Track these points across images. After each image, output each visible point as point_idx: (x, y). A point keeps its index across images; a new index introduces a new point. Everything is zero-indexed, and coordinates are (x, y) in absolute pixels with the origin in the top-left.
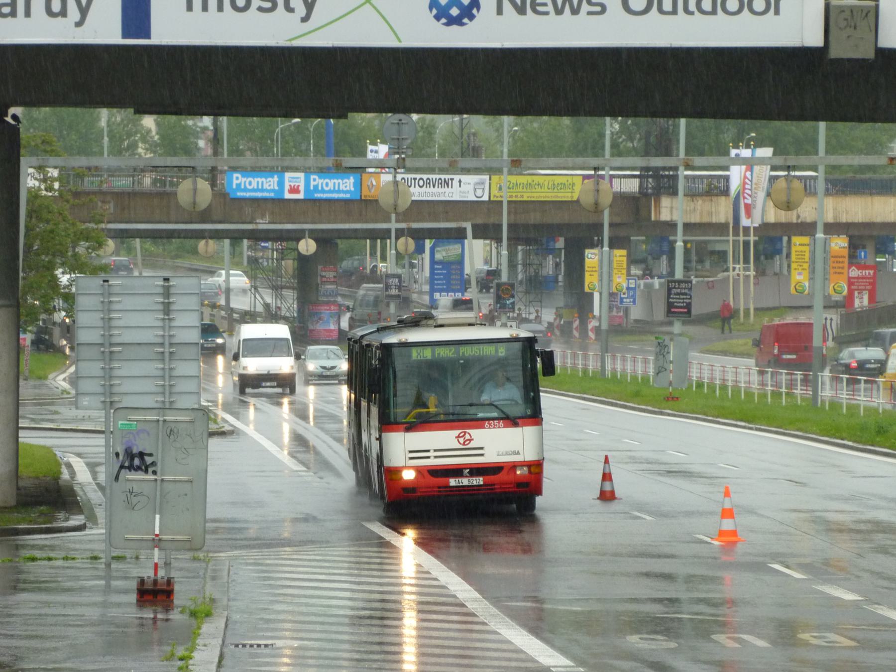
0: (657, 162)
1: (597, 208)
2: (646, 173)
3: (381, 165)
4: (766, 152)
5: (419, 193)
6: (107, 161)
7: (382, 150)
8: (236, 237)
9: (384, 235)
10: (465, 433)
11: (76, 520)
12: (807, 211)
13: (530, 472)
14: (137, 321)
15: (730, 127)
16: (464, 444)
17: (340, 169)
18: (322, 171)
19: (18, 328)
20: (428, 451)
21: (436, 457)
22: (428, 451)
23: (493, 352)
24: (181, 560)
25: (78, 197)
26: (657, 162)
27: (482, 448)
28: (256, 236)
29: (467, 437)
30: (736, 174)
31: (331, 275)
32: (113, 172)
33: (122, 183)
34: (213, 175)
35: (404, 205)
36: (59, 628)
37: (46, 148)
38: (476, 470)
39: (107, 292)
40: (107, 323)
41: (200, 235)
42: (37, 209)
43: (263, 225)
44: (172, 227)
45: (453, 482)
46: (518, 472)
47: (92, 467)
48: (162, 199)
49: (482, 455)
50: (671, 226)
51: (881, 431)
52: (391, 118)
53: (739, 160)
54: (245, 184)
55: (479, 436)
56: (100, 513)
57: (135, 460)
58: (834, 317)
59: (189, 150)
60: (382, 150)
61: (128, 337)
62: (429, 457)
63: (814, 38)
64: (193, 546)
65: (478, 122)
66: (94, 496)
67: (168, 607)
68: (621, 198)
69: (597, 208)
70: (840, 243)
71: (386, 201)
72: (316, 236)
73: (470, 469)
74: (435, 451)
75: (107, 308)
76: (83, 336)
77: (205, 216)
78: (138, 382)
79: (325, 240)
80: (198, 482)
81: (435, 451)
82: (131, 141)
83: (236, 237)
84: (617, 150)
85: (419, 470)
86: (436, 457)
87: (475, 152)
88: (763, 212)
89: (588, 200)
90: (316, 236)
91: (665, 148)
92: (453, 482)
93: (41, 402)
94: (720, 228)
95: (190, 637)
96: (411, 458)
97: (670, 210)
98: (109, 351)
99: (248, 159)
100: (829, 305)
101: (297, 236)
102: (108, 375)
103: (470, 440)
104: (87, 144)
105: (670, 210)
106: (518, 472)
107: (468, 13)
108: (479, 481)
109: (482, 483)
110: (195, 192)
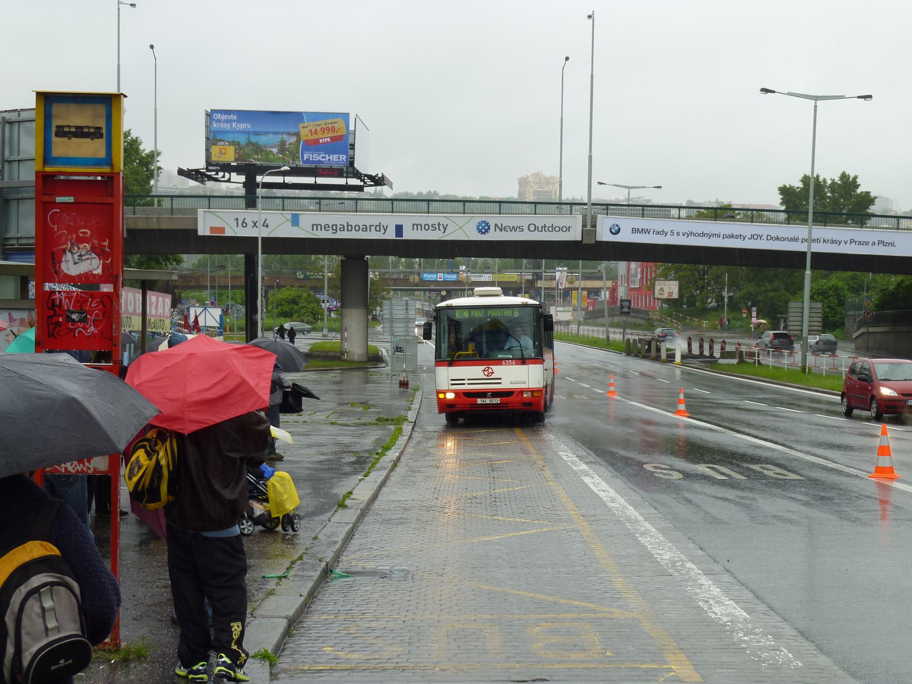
0: (537, 271)
1: (521, 283)
2: (534, 274)
3: (463, 271)
4: (566, 269)
5: (473, 279)
6: (391, 270)
7: (464, 267)
8: (425, 291)
9: (464, 290)
11: (383, 365)
12: (576, 284)
14: (399, 313)
15: (556, 261)
17: (453, 273)
18: (448, 273)
19: (368, 314)
23: (511, 314)
24: (411, 376)
25: (384, 280)
26: (537, 271)
28: (430, 290)
29: (490, 371)
30: (558, 274)
32: (393, 273)
33: (395, 276)
34: (419, 274)
35: (469, 282)
37: (375, 267)
38: (496, 394)
39: (391, 305)
40: (391, 313)
41: (415, 290)
42: (373, 283)
43: (432, 287)
44: (406, 286)
45: (479, 401)
47: (387, 351)
48: (405, 281)
50: (541, 288)
51: (595, 342)
52: (467, 259)
53: (559, 271)
54: (427, 277)
56: (389, 363)
57: (398, 349)
58: (583, 312)
59: (413, 267)
60: (464, 267)
61: (397, 317)
63: (579, 238)
64: (413, 372)
65: (489, 260)
66: (388, 359)
67: (407, 388)
68: (527, 280)
69: (521, 283)
70: (585, 293)
71: (465, 281)
75: (391, 309)
76: (385, 316)
77: (417, 285)
78: (399, 329)
80: (415, 355)
82: (396, 265)
83: (425, 291)
84: (526, 268)
85: (457, 393)
87: (489, 268)
88: (565, 285)
89: (518, 281)
91: (539, 267)
92: (479, 401)
93: (373, 334)
94: (553, 289)
95: (413, 396)
97: (540, 284)
98: (392, 320)
99: (428, 270)
100: (583, 309)
101: (441, 290)
102: (392, 327)
104: (386, 266)
105: (540, 284)
107: (487, 231)
108: (497, 401)
110: (414, 278)
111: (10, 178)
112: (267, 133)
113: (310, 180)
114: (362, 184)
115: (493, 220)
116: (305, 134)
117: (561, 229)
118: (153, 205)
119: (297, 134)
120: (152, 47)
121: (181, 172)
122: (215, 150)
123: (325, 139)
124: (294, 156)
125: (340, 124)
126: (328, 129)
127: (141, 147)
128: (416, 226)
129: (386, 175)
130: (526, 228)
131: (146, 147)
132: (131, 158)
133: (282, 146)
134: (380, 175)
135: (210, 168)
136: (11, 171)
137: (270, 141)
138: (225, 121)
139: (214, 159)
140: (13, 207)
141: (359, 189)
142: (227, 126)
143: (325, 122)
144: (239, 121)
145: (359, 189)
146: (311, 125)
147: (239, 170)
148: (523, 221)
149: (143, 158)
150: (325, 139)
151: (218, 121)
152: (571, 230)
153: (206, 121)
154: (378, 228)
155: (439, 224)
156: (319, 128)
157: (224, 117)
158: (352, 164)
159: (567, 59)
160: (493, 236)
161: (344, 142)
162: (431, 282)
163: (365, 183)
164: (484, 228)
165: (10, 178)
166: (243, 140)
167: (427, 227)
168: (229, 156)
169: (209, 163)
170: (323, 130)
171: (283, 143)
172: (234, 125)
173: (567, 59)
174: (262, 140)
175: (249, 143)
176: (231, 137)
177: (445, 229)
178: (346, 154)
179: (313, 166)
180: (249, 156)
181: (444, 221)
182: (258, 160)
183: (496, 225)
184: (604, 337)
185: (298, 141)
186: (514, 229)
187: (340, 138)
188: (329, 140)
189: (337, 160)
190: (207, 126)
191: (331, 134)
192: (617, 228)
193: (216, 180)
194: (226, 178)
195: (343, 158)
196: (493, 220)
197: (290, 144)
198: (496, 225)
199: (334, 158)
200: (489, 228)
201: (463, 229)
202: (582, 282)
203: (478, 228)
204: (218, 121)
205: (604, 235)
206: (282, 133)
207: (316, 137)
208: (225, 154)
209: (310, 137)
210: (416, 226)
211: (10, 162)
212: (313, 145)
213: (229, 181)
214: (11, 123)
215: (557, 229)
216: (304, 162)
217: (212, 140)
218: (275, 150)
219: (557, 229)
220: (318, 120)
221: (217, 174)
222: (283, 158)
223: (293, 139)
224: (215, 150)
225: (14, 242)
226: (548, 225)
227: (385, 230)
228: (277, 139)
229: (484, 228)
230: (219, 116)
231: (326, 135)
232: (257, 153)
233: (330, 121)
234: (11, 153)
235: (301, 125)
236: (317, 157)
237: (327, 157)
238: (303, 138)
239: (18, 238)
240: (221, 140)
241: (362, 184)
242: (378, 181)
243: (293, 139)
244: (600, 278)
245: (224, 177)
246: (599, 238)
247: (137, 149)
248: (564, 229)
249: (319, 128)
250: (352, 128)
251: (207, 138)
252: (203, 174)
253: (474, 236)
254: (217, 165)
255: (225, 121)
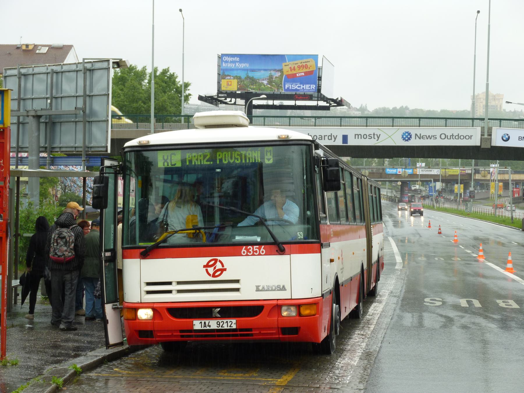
10: (216, 261)
13: (299, 314)
16: (214, 276)
20: (170, 283)
21: (179, 291)
22: (170, 283)
27: (237, 281)
29: (219, 266)
30: (491, 170)
31: (407, 189)
36: (32, 380)
38: (228, 310)
43: (393, 179)
45: (197, 325)
46: (285, 314)
49: (238, 290)
53: (492, 167)
55: (234, 265)
62: (170, 292)
63: (478, 144)
70: (501, 184)
71: (403, 175)
72: (401, 181)
73: (222, 308)
74: (179, 283)
79: (403, 182)
81: (179, 283)
85: (156, 309)
86: (179, 291)
90: (401, 181)
92: (197, 325)
96: (149, 292)
101: (397, 181)
103: (223, 270)
106: (285, 314)
107: (409, 139)
108: (231, 324)
109: (234, 327)
111: (57, 108)
112: (260, 70)
113: (291, 103)
114: (328, 105)
115: (413, 131)
116: (287, 70)
117: (465, 137)
118: (181, 122)
119: (281, 71)
120: (181, 10)
121: (201, 98)
122: (224, 82)
123: (300, 73)
124: (278, 86)
125: (311, 63)
126: (303, 67)
127: (177, 80)
128: (357, 136)
129: (344, 98)
130: (438, 137)
131: (180, 81)
132: (170, 88)
133: (270, 80)
134: (339, 99)
135: (220, 95)
136: (57, 104)
137: (262, 76)
138: (231, 62)
139: (223, 89)
140: (58, 127)
141: (327, 108)
142: (232, 66)
143: (300, 61)
144: (240, 62)
145: (327, 108)
146: (291, 64)
147: (241, 96)
148: (436, 131)
149: (178, 87)
150: (300, 73)
151: (226, 62)
152: (472, 137)
153: (219, 62)
154: (330, 137)
155: (374, 135)
156: (296, 66)
157: (230, 59)
158: (319, 90)
159: (478, 12)
160: (414, 142)
161: (315, 76)
162: (392, 175)
163: (330, 104)
164: (407, 137)
165: (57, 108)
166: (243, 75)
167: (365, 137)
168: (233, 86)
169: (219, 92)
170: (299, 67)
171: (271, 77)
172: (237, 64)
173: (478, 12)
174: (256, 75)
175: (248, 77)
176: (235, 73)
177: (378, 138)
178: (315, 84)
179: (294, 93)
180: (248, 87)
181: (378, 132)
182: (254, 89)
183: (416, 135)
184: (510, 216)
185: (282, 76)
186: (429, 137)
187: (311, 73)
188: (303, 74)
189: (309, 88)
190: (219, 66)
191: (305, 70)
192: (507, 137)
193: (226, 103)
194: (233, 102)
195: (313, 87)
196: (413, 131)
197: (276, 77)
198: (416, 135)
199: (307, 87)
200: (411, 137)
201: (391, 137)
202: (512, 175)
203: (403, 137)
204: (226, 62)
205: (497, 142)
206: (271, 70)
207: (294, 72)
208: (231, 85)
209: (290, 73)
210: (357, 136)
211: (56, 98)
212: (292, 78)
213: (235, 104)
214: (57, 73)
215: (462, 137)
216: (285, 90)
217: (222, 75)
218: (265, 82)
219: (462, 137)
220: (295, 60)
221: (226, 99)
222: (271, 88)
223: (278, 74)
224: (224, 82)
225: (58, 150)
226: (455, 135)
227: (335, 139)
228: (267, 74)
229: (407, 137)
230: (227, 59)
231: (301, 71)
232: (252, 84)
233: (304, 60)
234: (57, 93)
235: (284, 64)
236: (295, 86)
237: (302, 87)
238: (285, 73)
239: (75, 147)
240: (228, 76)
241: (328, 105)
242: (339, 103)
243: (278, 74)
244: (422, 176)
245: (231, 101)
246: (494, 144)
247: (174, 81)
248: (467, 137)
249: (296, 66)
250: (320, 65)
251: (219, 74)
252: (216, 100)
253: (400, 143)
254: (226, 93)
255: (231, 62)
